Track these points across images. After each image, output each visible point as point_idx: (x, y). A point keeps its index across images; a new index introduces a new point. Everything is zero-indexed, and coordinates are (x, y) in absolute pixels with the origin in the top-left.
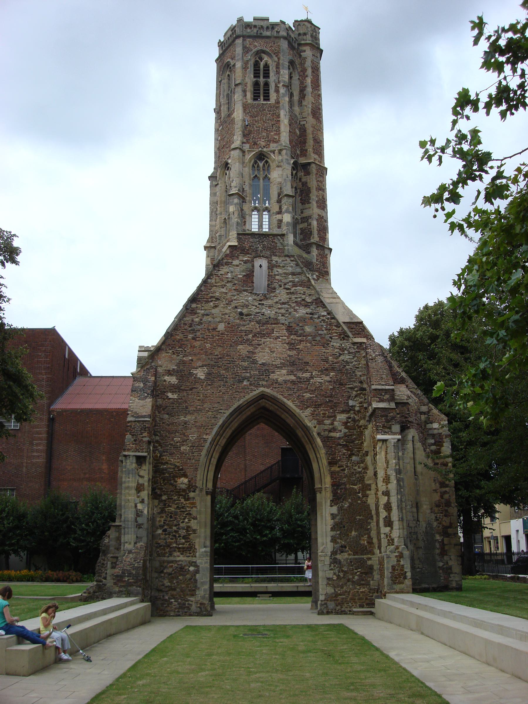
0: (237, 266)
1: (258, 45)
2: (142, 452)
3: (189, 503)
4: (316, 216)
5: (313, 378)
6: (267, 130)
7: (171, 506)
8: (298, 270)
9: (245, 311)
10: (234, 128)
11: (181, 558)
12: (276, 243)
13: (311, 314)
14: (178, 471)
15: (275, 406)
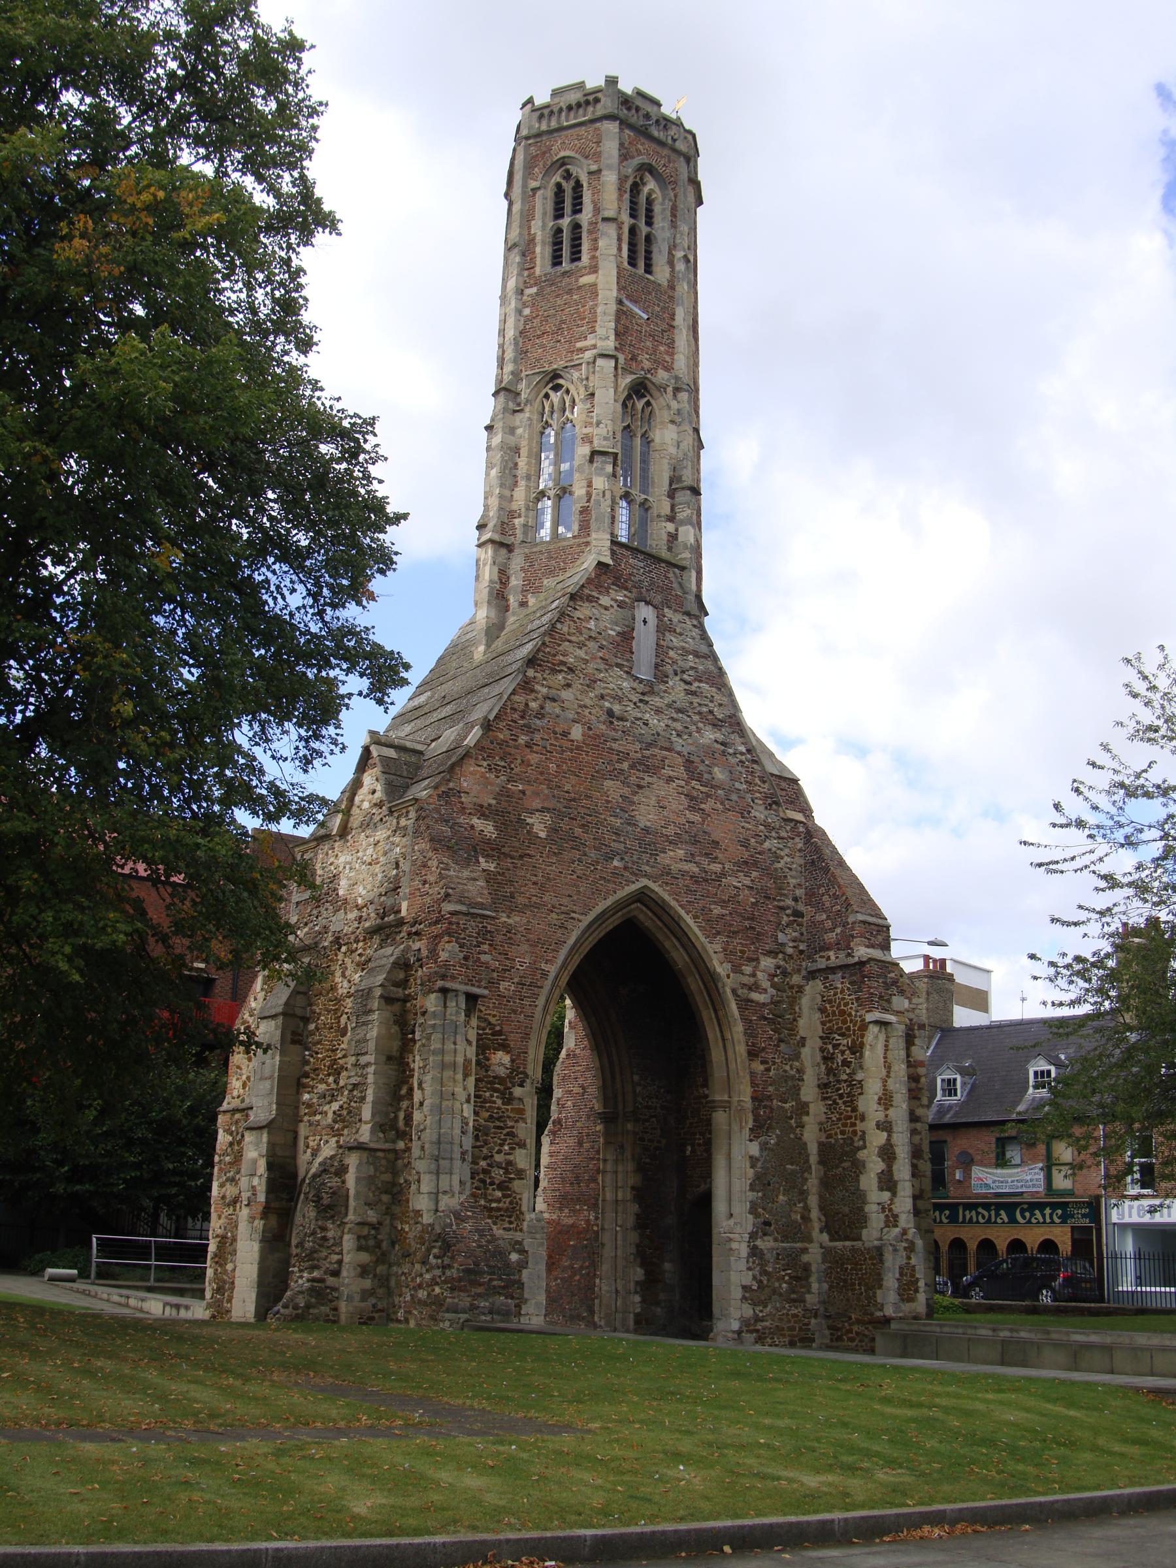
0: (606, 608)
1: (645, 153)
2: (479, 987)
9: (617, 708)
12: (671, 582)
13: (723, 744)
14: (493, 1035)
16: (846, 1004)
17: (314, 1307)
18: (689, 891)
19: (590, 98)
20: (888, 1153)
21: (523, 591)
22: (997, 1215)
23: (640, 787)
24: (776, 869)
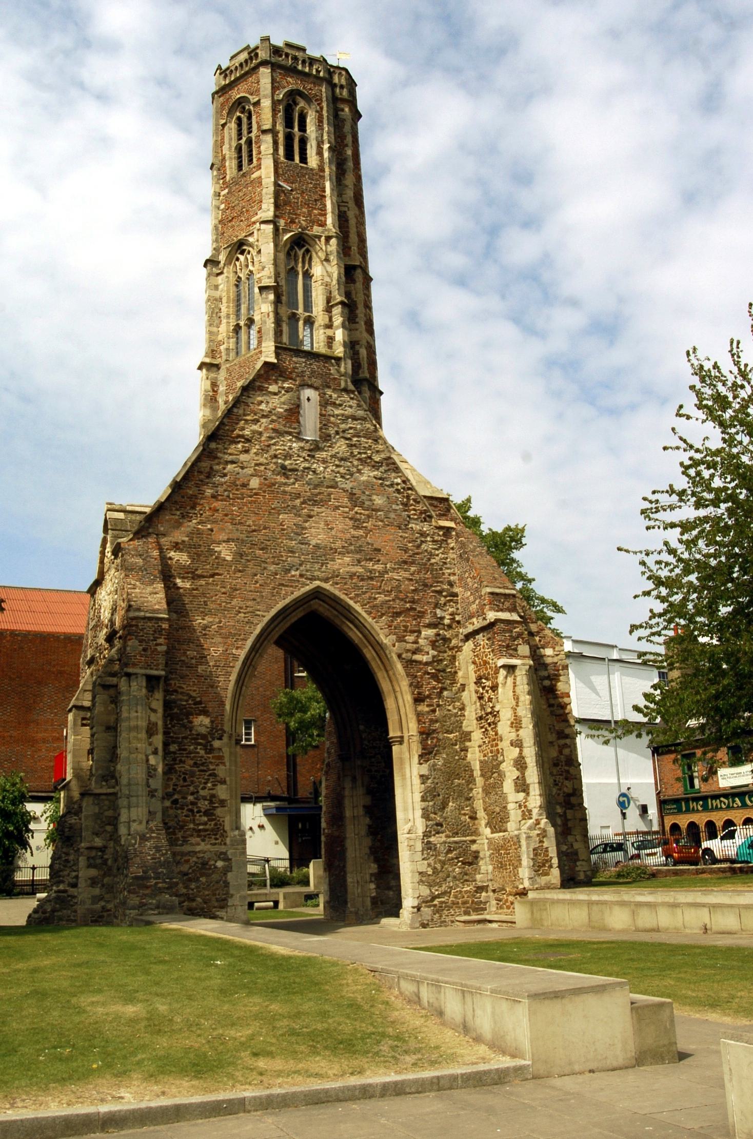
0: (275, 394)
1: (291, 83)
2: (156, 670)
3: (213, 757)
4: (364, 342)
5: (387, 573)
6: (308, 205)
7: (184, 762)
8: (361, 413)
10: (260, 194)
11: (203, 847)
14: (194, 704)
15: (333, 610)
16: (486, 656)
17: (58, 911)
18: (356, 587)
19: (253, 53)
20: (520, 764)
21: (226, 393)
22: (734, 801)
23: (310, 516)
24: (432, 564)
